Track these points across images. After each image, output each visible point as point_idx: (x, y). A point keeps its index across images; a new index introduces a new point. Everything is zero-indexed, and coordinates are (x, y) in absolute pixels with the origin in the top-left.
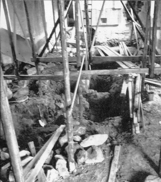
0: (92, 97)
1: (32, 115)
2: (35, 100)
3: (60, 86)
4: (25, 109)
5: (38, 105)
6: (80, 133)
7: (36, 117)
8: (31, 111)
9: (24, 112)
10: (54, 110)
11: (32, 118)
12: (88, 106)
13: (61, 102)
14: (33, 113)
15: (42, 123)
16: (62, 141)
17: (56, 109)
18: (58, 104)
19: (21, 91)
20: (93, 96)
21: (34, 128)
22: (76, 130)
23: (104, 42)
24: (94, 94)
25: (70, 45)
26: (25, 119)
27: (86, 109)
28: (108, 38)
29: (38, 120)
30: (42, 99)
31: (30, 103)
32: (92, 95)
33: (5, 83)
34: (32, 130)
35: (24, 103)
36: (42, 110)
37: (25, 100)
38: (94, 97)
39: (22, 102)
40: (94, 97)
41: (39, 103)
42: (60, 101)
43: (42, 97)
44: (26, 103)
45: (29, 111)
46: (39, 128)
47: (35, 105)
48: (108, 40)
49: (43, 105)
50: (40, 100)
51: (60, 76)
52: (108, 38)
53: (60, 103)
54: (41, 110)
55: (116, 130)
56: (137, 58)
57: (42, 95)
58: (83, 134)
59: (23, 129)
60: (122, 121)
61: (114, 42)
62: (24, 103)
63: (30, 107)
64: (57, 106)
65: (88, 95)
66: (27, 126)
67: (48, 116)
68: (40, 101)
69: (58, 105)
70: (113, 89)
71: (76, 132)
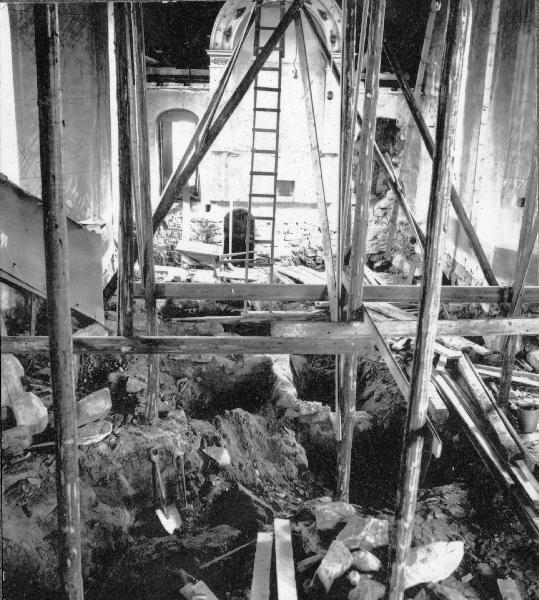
0: (315, 429)
1: (131, 492)
2: (140, 435)
3: (189, 390)
4: (109, 470)
5: (156, 453)
6: (371, 540)
7: (144, 502)
8: (127, 477)
9: (103, 482)
10: (199, 475)
11: (128, 502)
12: (303, 459)
13: (219, 445)
14: (135, 485)
15: (170, 523)
16: (327, 572)
17: (205, 473)
18: (210, 451)
19: (89, 404)
20: (319, 423)
21: (140, 542)
22: (360, 532)
23: (283, 255)
24: (322, 418)
25: (183, 258)
26: (104, 508)
27: (301, 467)
28: (294, 246)
29: (153, 510)
30: (162, 433)
31: (126, 447)
32: (315, 420)
33: (13, 369)
34: (134, 548)
35: (103, 447)
36: (165, 474)
37: (104, 436)
38: (323, 429)
39: (93, 445)
40: (323, 429)
41: (158, 446)
42: (215, 442)
43: (159, 425)
44: (113, 447)
45: (122, 478)
46: (158, 540)
47: (146, 454)
48: (297, 250)
49: (169, 453)
50: (157, 436)
51: (292, 338)
52: (294, 246)
53: (215, 448)
54: (162, 471)
55: (463, 528)
56: (492, 292)
57: (156, 419)
58: (380, 544)
59: (103, 545)
60: (469, 497)
61: (314, 258)
62: (103, 447)
63: (126, 461)
64: (206, 458)
65: (303, 421)
66: (118, 532)
67: (182, 495)
68: (158, 441)
69: (213, 456)
70: (378, 401)
71: (358, 537)
